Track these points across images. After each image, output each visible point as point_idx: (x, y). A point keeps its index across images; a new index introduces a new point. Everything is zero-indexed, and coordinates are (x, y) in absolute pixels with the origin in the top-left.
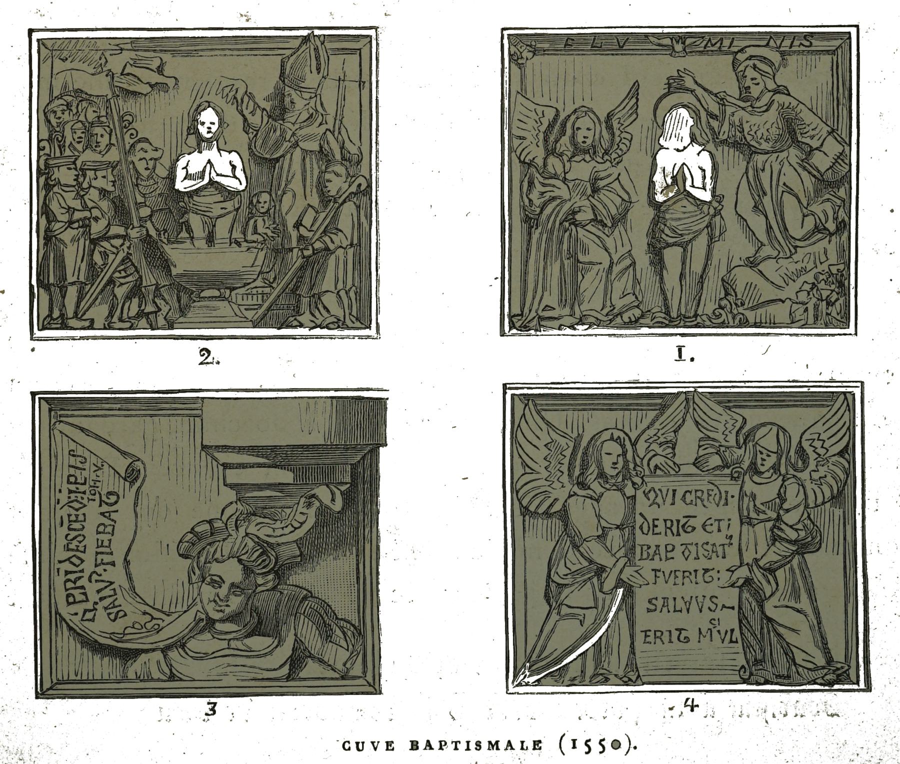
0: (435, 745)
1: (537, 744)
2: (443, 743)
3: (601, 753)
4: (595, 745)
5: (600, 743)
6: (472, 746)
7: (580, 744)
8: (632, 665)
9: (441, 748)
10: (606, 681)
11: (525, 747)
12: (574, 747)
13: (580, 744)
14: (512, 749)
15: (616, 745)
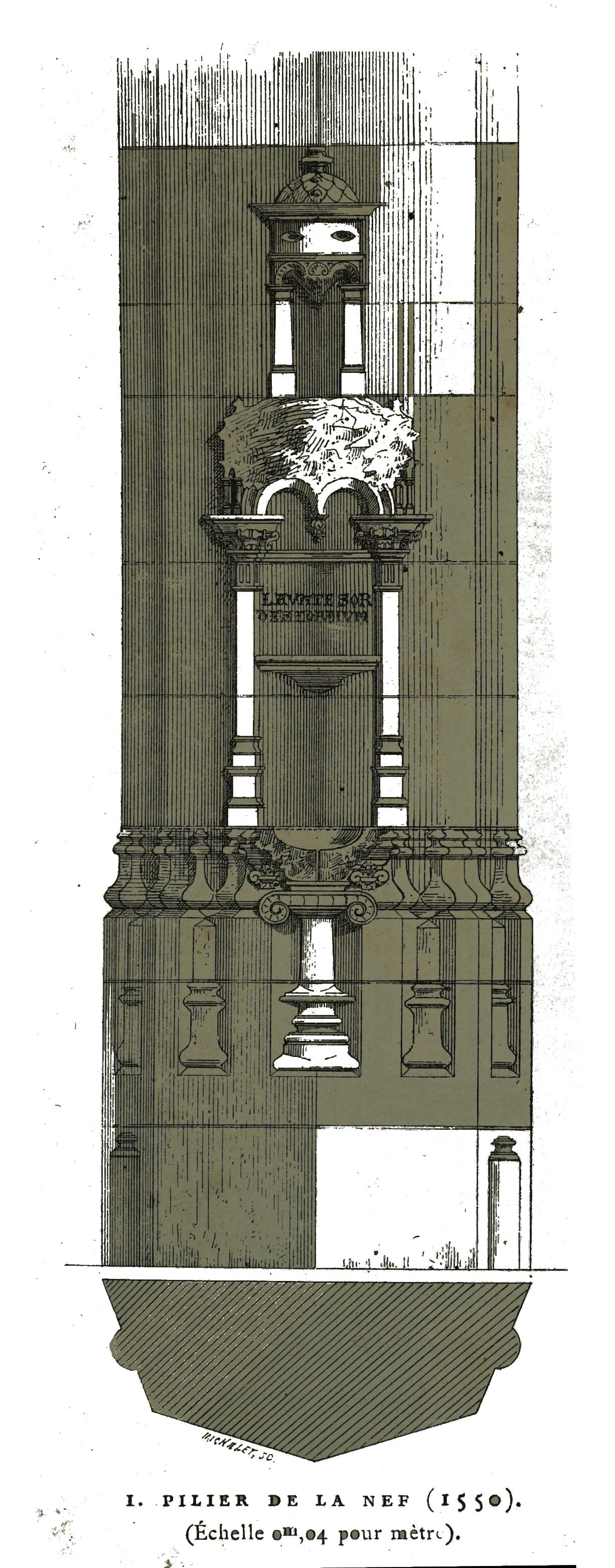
0: (396, 1500)
1: (167, 1500)
2: (169, 1499)
3: (460, 1510)
4: (469, 1500)
5: (477, 1500)
6: (216, 1501)
7: (453, 1500)
8: (162, 905)
9: (401, 1505)
10: (250, 1267)
11: (197, 1502)
12: (445, 1504)
13: (453, 1500)
14: (341, 1505)
15: (495, 1501)
